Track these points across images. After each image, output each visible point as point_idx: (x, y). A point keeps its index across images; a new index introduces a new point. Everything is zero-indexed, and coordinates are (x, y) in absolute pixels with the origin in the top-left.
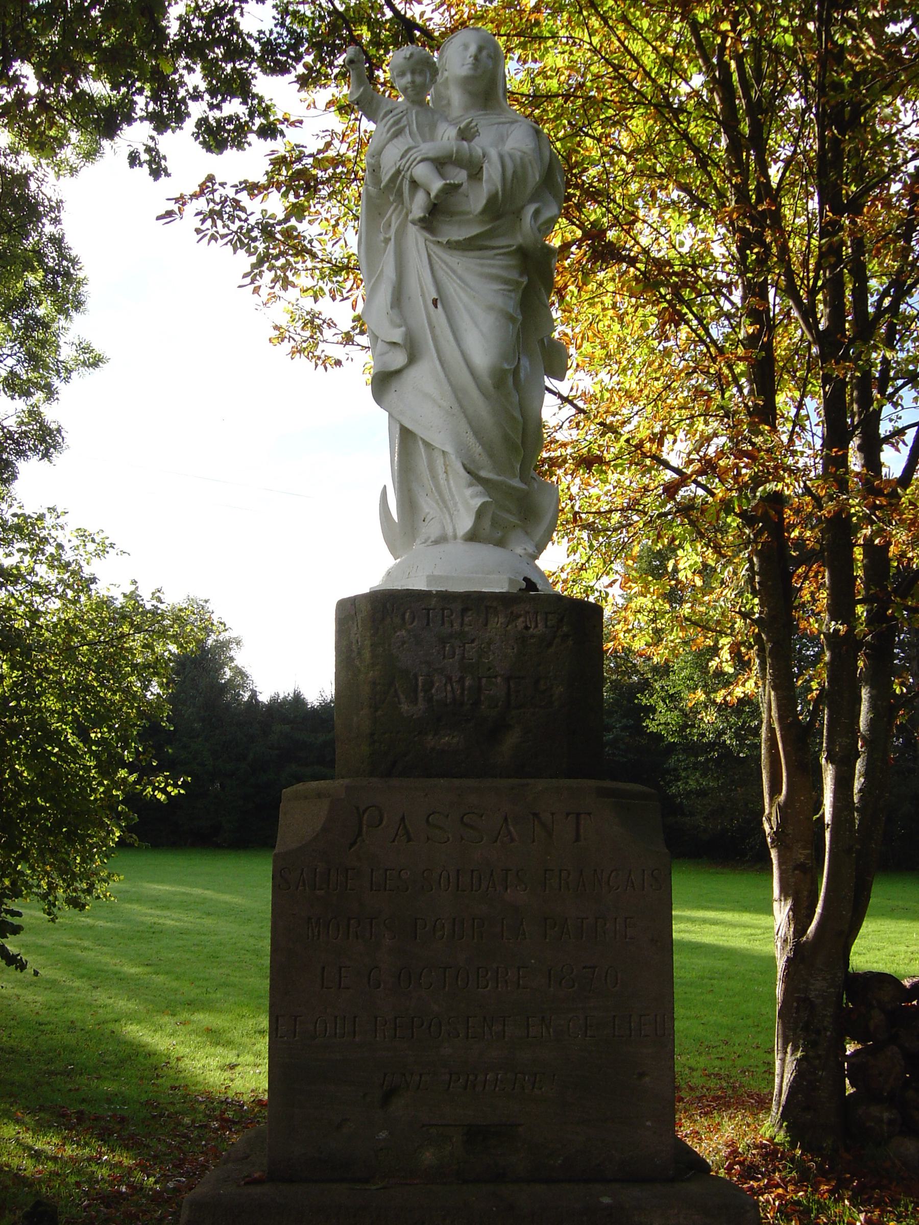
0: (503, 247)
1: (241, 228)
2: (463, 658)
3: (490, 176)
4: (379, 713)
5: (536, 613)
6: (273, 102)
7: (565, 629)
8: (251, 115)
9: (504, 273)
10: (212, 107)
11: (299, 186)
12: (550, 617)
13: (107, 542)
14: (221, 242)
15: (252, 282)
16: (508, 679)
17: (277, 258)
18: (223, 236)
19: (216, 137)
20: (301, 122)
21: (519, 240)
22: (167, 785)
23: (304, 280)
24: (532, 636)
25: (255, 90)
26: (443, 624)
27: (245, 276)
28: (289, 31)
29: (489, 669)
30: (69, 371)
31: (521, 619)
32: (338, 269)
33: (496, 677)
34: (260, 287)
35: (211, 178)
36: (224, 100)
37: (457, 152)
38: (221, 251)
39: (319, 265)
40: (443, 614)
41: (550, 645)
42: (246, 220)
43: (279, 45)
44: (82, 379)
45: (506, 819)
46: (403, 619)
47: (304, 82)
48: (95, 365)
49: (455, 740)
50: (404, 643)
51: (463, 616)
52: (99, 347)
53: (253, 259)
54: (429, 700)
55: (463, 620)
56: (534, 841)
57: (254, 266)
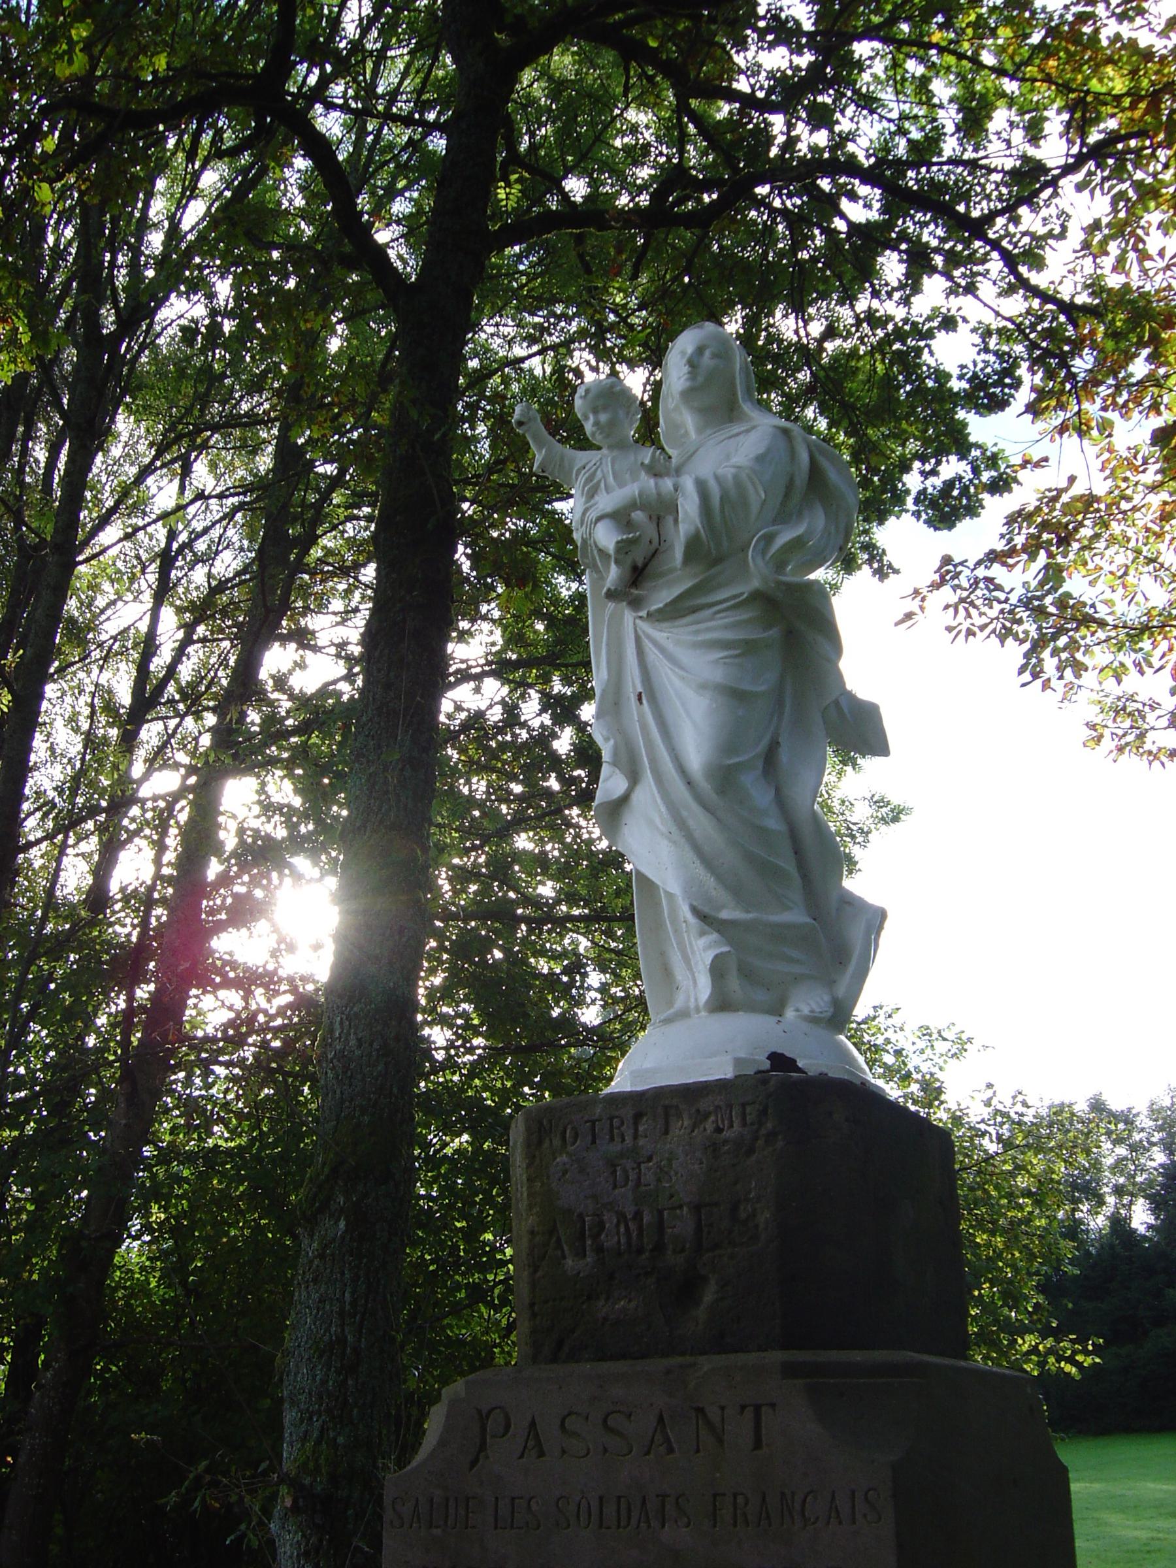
0: (721, 602)
1: (1002, 611)
2: (638, 1183)
3: (686, 512)
4: (539, 1274)
5: (730, 1107)
6: (1000, 446)
7: (769, 1125)
8: (976, 471)
9: (729, 635)
10: (925, 475)
11: (1049, 542)
12: (749, 1109)
13: (964, 1037)
14: (981, 635)
15: (1035, 676)
16: (697, 1208)
17: (1055, 637)
18: (982, 628)
19: (946, 509)
20: (1046, 459)
21: (755, 584)
22: (1074, 1352)
23: (1100, 657)
24: (726, 1142)
25: (972, 439)
26: (612, 1139)
27: (1021, 671)
28: (996, 353)
29: (672, 1196)
30: (866, 833)
31: (712, 1118)
32: (1138, 632)
33: (680, 1207)
34: (1049, 680)
35: (947, 560)
36: (938, 463)
37: (640, 495)
38: (986, 646)
39: (1113, 634)
40: (611, 1125)
41: (751, 1151)
42: (1006, 601)
43: (988, 376)
44: (882, 837)
45: (661, 1419)
46: (564, 1138)
47: (1034, 409)
48: (896, 819)
49: (633, 1305)
50: (565, 1172)
51: (636, 1124)
52: (895, 800)
53: (1027, 646)
54: (599, 1249)
55: (636, 1130)
56: (698, 1451)
57: (1027, 656)
